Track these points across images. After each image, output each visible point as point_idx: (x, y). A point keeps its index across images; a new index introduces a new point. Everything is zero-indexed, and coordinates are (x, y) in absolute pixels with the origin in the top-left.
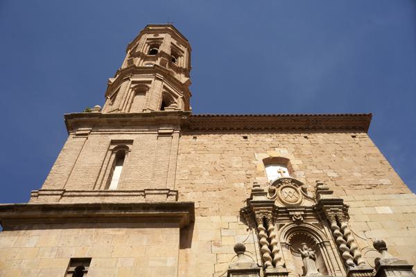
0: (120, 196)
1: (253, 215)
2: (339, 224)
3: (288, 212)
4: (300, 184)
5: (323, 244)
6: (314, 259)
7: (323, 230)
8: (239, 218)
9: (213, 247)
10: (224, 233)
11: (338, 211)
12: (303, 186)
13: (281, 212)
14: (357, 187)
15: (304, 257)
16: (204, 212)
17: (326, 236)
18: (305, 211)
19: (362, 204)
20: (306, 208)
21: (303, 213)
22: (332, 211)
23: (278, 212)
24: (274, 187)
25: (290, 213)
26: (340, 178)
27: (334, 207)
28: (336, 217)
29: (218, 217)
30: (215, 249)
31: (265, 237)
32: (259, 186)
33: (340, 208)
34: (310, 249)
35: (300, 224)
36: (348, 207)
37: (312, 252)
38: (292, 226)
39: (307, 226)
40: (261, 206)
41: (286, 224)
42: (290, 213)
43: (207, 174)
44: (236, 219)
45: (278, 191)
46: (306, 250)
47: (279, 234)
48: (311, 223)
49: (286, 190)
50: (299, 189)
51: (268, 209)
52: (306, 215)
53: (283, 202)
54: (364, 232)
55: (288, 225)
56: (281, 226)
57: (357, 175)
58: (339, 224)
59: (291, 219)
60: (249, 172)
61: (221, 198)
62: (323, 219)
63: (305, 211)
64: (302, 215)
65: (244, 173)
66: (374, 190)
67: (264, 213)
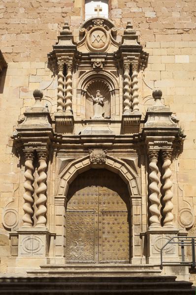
0: (87, 263)
1: (122, 61)
2: (131, 74)
3: (90, 58)
4: (111, 26)
5: (113, 92)
6: (102, 105)
7: (117, 79)
8: (47, 64)
9: (21, 92)
10: (32, 79)
11: (134, 59)
12: (113, 29)
13: (85, 59)
14: (169, 31)
15: (94, 103)
16: (17, 58)
17: (118, 84)
18: (106, 58)
19: (164, 51)
20: (108, 54)
21: (103, 60)
22: (128, 59)
23: (81, 59)
24: (84, 30)
25: (92, 60)
26: (156, 19)
27: (64, 55)
28: (131, 66)
29: (28, 63)
30: (22, 94)
31: (129, 98)
32: (131, 27)
33: (136, 56)
34: (102, 96)
35: (99, 72)
36: (147, 55)
37: (102, 99)
38: (91, 73)
39: (105, 73)
40: (64, 51)
41: (87, 71)
42: (92, 60)
43: (22, 11)
44: (44, 64)
45: (88, 33)
46: (98, 96)
47: (76, 80)
48: (109, 71)
49: (96, 33)
50: (109, 33)
51: (70, 56)
52: (106, 63)
53: (89, 48)
54: (155, 81)
55: (88, 71)
56: (81, 73)
57: (176, 15)
58: (131, 74)
59: (92, 66)
60: (65, 10)
61: (33, 42)
62: (120, 67)
63: (106, 58)
64: (102, 62)
65: (59, 10)
66: (185, 35)
67: (65, 59)
